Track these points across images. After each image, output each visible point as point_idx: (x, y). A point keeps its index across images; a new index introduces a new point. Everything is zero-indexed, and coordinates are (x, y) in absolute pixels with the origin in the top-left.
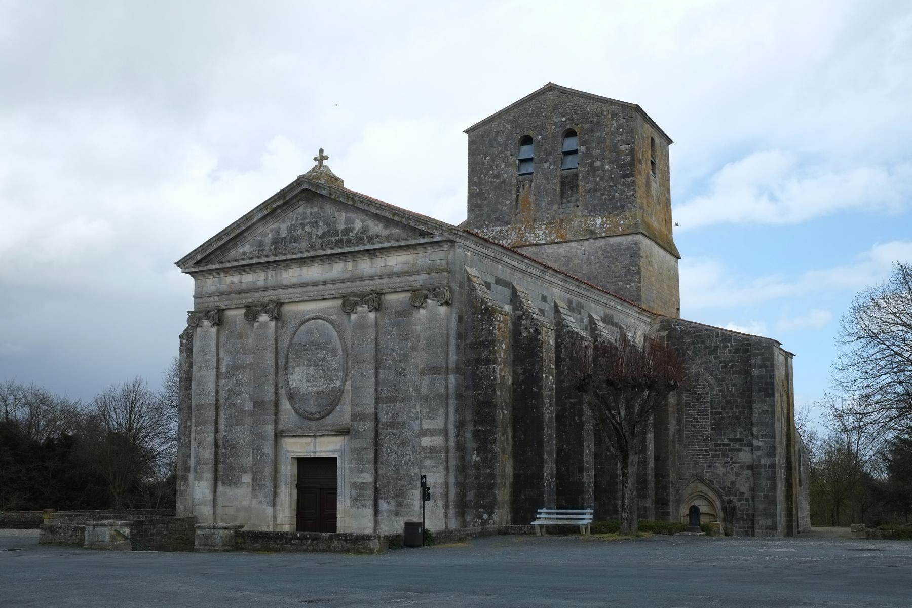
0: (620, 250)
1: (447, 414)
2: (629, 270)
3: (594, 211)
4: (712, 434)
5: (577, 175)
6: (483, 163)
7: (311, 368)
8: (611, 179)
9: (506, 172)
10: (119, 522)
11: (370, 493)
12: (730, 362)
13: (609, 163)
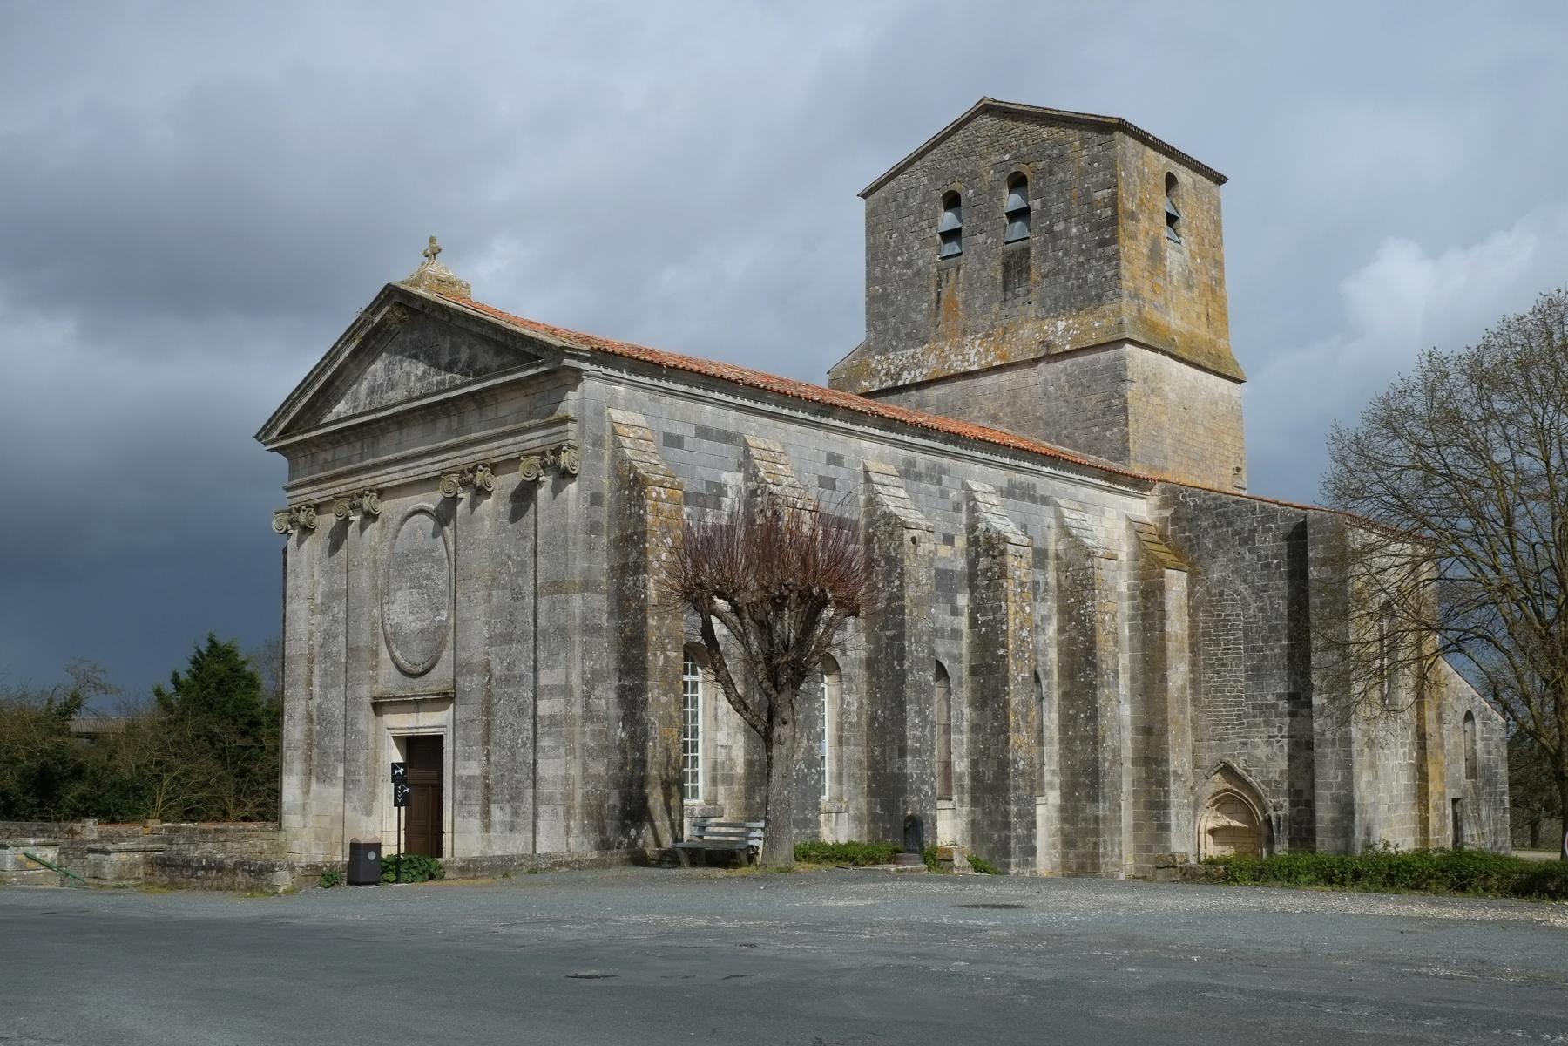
0: (1094, 372)
2: (1110, 406)
3: (1056, 308)
4: (1247, 687)
5: (1027, 250)
6: (887, 245)
7: (415, 591)
8: (1081, 251)
9: (921, 257)
10: (32, 841)
11: (477, 793)
12: (1275, 557)
13: (1077, 224)
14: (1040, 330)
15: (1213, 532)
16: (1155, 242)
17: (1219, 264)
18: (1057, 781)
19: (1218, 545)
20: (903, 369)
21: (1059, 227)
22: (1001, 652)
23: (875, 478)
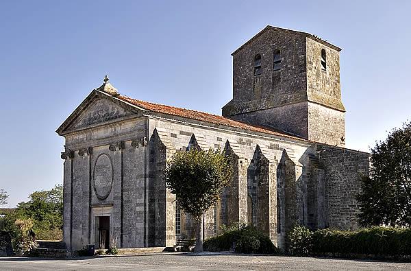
1: (145, 196)
8: (295, 73)
17: (338, 76)
19: (333, 162)
21: (289, 66)
23: (231, 144)
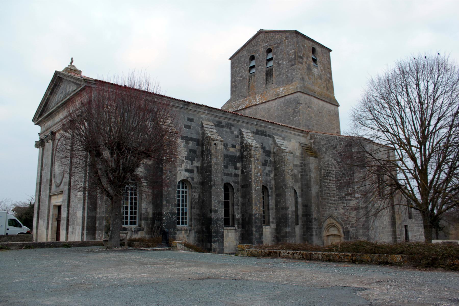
2: (295, 111)
3: (280, 84)
5: (272, 69)
6: (236, 71)
14: (276, 91)
15: (325, 146)
16: (309, 65)
18: (274, 221)
20: (240, 105)
21: (280, 62)
22: (250, 180)
23: (205, 126)
